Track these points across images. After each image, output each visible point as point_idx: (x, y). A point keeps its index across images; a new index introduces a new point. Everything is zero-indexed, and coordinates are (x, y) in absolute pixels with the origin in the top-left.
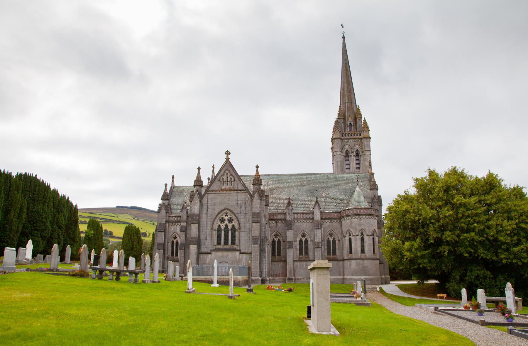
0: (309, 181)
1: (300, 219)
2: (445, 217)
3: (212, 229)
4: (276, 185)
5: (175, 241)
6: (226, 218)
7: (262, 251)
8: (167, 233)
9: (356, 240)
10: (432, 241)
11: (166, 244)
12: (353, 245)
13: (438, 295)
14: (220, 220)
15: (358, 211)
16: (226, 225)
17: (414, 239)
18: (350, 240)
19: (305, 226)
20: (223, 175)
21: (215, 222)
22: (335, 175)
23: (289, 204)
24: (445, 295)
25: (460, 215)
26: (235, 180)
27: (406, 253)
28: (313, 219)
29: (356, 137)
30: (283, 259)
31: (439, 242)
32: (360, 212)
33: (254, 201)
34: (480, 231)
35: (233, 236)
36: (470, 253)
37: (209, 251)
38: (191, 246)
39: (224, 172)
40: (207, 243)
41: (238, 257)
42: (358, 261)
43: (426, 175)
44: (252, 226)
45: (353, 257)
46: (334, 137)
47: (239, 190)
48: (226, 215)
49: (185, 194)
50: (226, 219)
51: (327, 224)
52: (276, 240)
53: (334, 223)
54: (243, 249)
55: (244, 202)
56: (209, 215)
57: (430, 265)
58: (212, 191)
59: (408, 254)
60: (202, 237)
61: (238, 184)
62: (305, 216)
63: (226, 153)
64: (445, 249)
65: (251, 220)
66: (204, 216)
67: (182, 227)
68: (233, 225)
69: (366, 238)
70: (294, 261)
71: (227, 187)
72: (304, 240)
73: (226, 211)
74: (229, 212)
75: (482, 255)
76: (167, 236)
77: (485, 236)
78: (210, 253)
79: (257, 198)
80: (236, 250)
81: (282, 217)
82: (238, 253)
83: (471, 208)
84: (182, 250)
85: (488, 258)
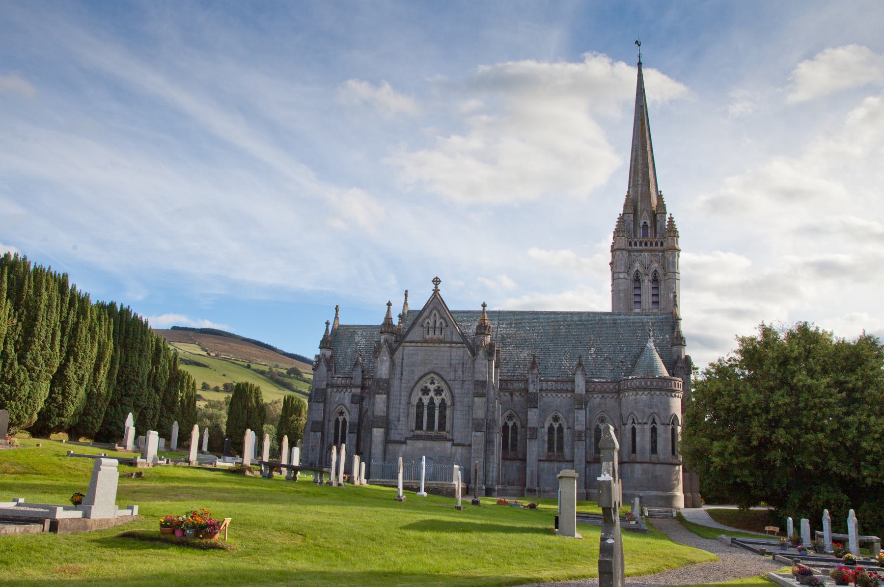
0: (569, 326)
1: (552, 390)
2: (778, 406)
3: (409, 403)
4: (513, 331)
5: (341, 419)
6: (432, 387)
7: (488, 442)
8: (327, 405)
9: (643, 431)
10: (755, 443)
11: (326, 422)
12: (638, 439)
13: (767, 528)
14: (422, 390)
15: (649, 383)
16: (432, 399)
17: (729, 437)
18: (634, 429)
19: (560, 401)
20: (428, 317)
21: (414, 394)
22: (613, 317)
23: (534, 365)
24: (777, 529)
25: (801, 405)
26: (447, 326)
27: (715, 459)
28: (573, 391)
29: (654, 247)
30: (520, 456)
31: (766, 444)
32: (652, 384)
33: (478, 361)
34: (833, 431)
35: (443, 417)
36: (816, 465)
37: (403, 439)
38: (375, 430)
39: (431, 312)
40: (400, 427)
41: (449, 451)
42: (646, 465)
43: (757, 334)
44: (473, 402)
45: (638, 459)
46: (615, 247)
47: (454, 343)
48: (432, 383)
49: (357, 339)
50: (432, 389)
51: (596, 399)
52: (510, 424)
53: (608, 400)
54: (458, 437)
55: (461, 362)
56: (403, 381)
57: (753, 479)
58: (411, 342)
59: (716, 460)
60: (393, 416)
61: (452, 333)
62: (560, 386)
63: (433, 281)
64: (776, 456)
65: (471, 392)
66: (396, 383)
67: (353, 396)
68: (443, 400)
69: (660, 429)
70: (539, 461)
71: (434, 337)
72: (556, 426)
73: (432, 375)
74: (436, 377)
75: (834, 469)
76: (327, 410)
77: (840, 439)
78: (404, 443)
79: (483, 357)
80: (445, 439)
81: (522, 385)
82: (449, 444)
83: (820, 395)
84: (352, 435)
85: (843, 473)
